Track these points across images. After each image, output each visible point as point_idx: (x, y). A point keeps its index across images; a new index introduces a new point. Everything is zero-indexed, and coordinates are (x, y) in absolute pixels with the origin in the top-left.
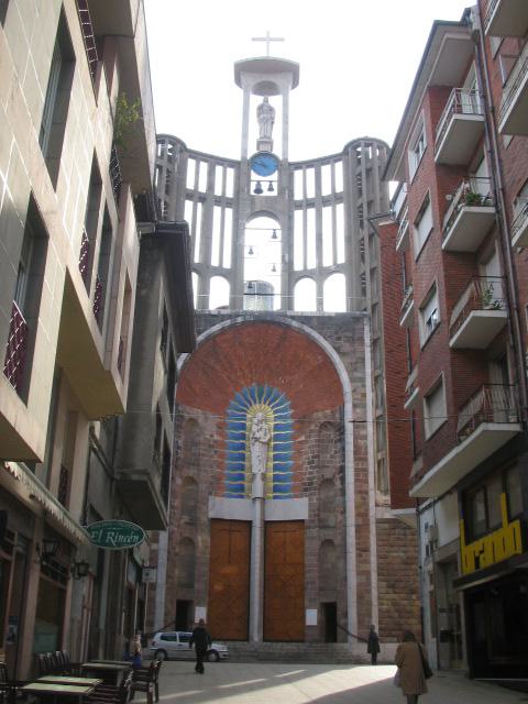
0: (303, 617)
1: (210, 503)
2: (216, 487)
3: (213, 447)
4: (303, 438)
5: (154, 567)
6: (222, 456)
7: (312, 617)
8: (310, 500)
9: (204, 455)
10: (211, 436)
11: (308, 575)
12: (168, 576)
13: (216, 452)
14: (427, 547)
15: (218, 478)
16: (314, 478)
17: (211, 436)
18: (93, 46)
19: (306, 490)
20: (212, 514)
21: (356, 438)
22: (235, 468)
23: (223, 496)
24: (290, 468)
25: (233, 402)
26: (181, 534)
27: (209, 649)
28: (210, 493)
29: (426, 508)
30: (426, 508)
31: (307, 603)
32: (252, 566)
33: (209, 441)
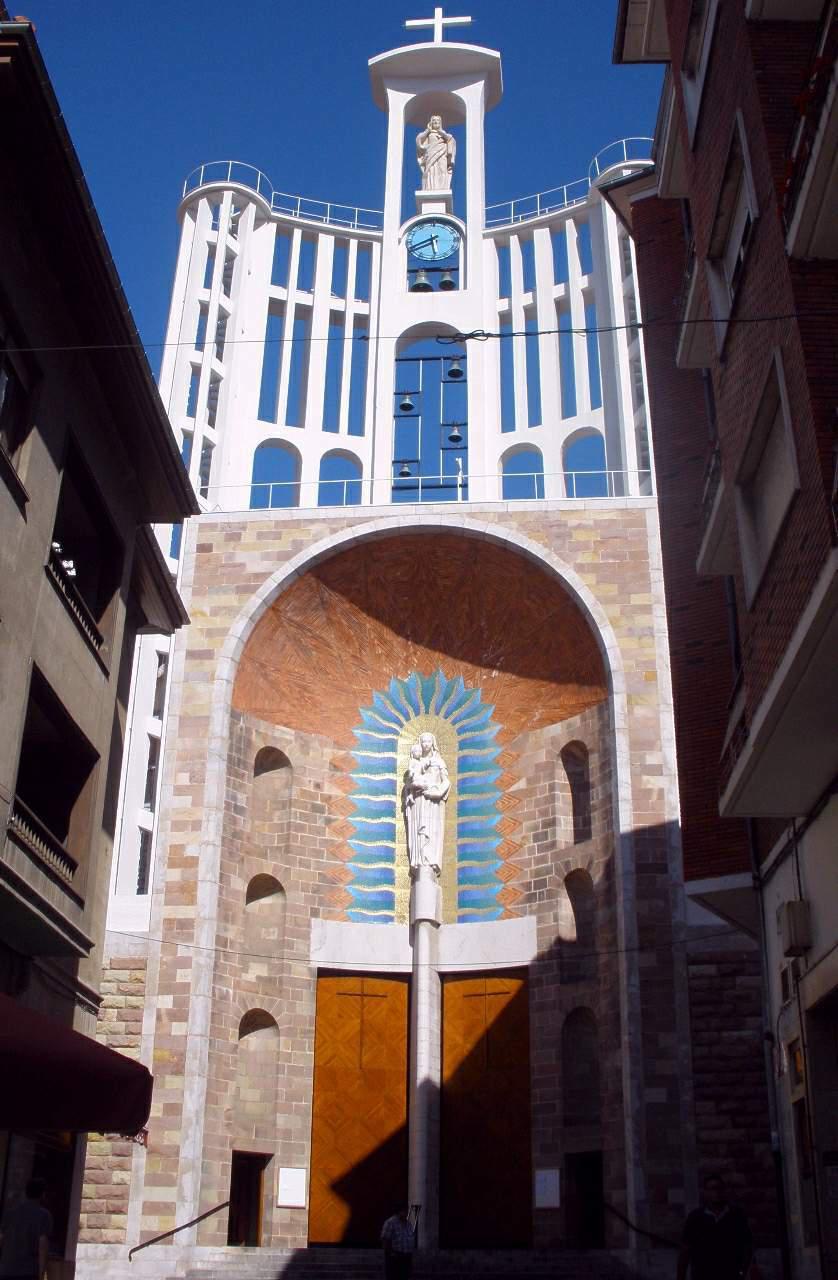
0: (527, 1188)
1: (315, 934)
2: (326, 898)
3: (320, 810)
4: (522, 784)
5: (179, 1070)
6: (336, 851)
7: (547, 1188)
8: (539, 921)
9: (301, 828)
10: (318, 786)
11: (536, 1091)
12: (211, 1098)
13: (328, 821)
14: (784, 975)
15: (330, 881)
16: (548, 871)
17: (318, 786)
18: (445, 39)
19: (530, 898)
20: (321, 959)
21: (635, 776)
22: (370, 858)
23: (347, 919)
24: (496, 855)
25: (367, 715)
26: (243, 1002)
27: (794, 161)
28: (315, 913)
29: (778, 863)
30: (778, 863)
31: (535, 1155)
32: (437, 1016)
33: (312, 796)
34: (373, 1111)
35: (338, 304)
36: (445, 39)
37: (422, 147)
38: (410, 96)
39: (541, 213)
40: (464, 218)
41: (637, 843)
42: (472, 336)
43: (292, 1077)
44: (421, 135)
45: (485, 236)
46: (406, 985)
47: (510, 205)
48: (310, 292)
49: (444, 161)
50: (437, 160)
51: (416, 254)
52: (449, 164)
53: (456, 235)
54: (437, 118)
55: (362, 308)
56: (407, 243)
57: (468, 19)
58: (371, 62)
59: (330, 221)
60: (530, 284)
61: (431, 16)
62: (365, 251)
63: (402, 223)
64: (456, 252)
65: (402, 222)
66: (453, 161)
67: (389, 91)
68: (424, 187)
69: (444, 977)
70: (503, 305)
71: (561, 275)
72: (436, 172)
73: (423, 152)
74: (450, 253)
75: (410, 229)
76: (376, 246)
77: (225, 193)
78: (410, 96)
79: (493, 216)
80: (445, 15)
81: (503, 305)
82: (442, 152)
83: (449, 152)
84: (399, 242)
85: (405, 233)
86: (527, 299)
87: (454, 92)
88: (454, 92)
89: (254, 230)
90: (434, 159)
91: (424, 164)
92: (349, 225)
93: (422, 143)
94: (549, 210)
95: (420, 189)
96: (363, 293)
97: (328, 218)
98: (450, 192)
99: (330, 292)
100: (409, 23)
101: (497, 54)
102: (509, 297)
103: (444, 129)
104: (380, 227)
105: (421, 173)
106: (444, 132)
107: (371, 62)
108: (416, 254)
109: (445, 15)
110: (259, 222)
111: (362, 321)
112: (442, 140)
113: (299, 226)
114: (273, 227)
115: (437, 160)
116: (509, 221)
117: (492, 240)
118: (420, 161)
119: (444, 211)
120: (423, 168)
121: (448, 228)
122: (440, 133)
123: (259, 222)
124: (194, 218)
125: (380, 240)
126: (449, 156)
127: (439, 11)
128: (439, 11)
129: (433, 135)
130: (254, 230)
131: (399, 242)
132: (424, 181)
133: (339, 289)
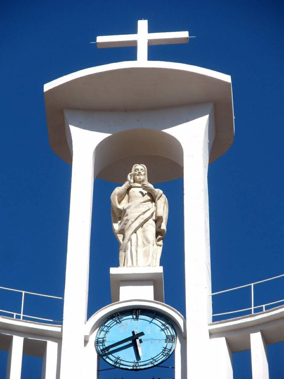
36: (152, 56)
37: (120, 207)
38: (102, 136)
39: (256, 311)
40: (182, 308)
43: (163, 194)
44: (118, 190)
45: (212, 334)
47: (251, 286)
49: (151, 228)
50: (142, 225)
51: (110, 360)
52: (158, 233)
53: (170, 332)
54: (140, 167)
56: (97, 343)
57: (185, 34)
58: (48, 87)
59: (24, 318)
61: (134, 30)
64: (171, 357)
65: (90, 313)
66: (164, 226)
67: (69, 125)
68: (121, 263)
73: (122, 214)
74: (161, 358)
75: (102, 323)
76: (51, 347)
77: (60, 329)
78: (102, 136)
82: (148, 214)
84: (86, 342)
85: (93, 330)
87: (164, 131)
88: (164, 131)
91: (122, 231)
92: (12, 316)
93: (120, 202)
94: (267, 308)
95: (117, 265)
97: (22, 315)
98: (160, 270)
100: (100, 39)
101: (227, 78)
103: (149, 181)
104: (58, 319)
105: (118, 244)
106: (151, 186)
107: (48, 87)
108: (110, 360)
112: (147, 197)
113: (19, 331)
115: (142, 225)
116: (250, 312)
117: (223, 339)
118: (116, 227)
119: (152, 298)
120: (120, 237)
121: (158, 322)
122: (145, 188)
125: (58, 338)
126: (158, 220)
127: (143, 25)
128: (143, 25)
129: (135, 191)
131: (86, 342)
132: (122, 254)
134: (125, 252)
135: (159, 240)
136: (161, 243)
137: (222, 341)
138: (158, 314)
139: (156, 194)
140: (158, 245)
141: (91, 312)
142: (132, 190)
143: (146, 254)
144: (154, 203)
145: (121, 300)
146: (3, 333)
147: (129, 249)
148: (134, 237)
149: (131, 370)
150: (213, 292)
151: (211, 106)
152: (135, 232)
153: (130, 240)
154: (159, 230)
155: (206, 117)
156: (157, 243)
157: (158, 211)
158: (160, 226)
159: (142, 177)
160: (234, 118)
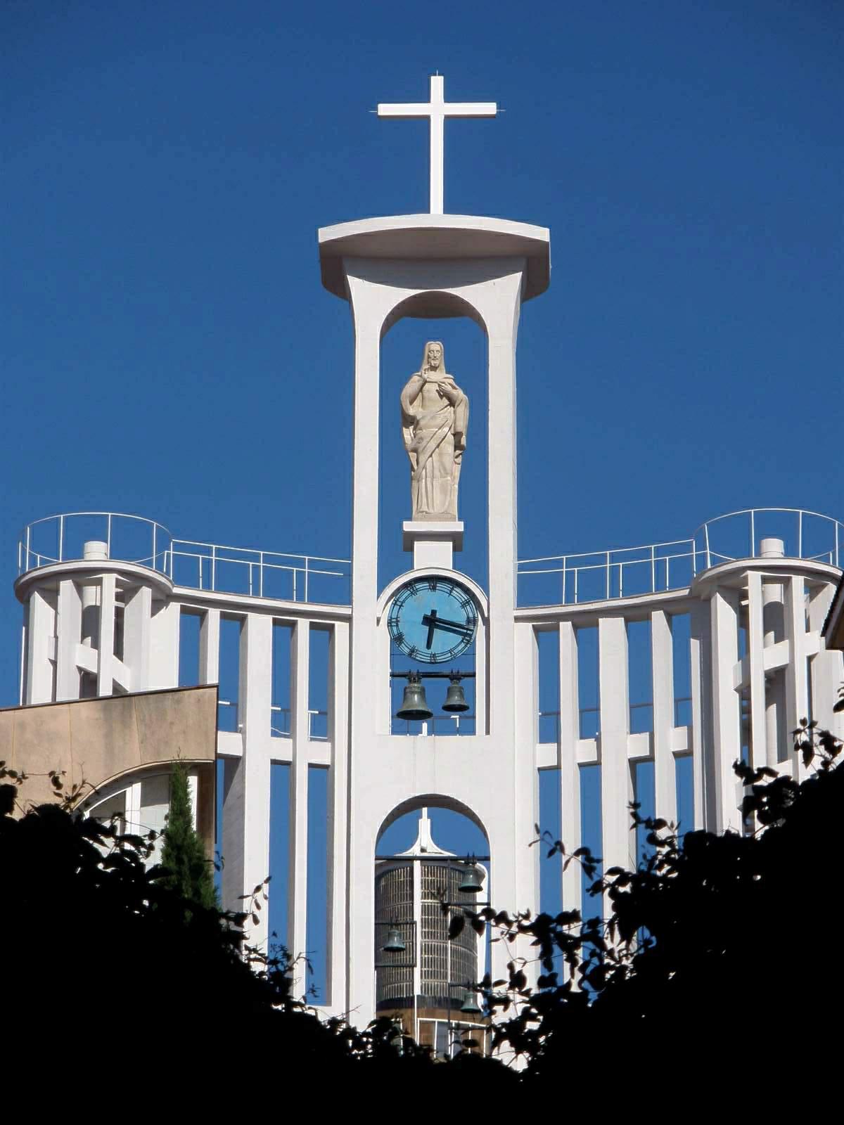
34: (80, 801)
35: (282, 749)
41: (783, 636)
42: (516, 1057)
45: (517, 619)
46: (218, 752)
48: (236, 730)
49: (448, 447)
52: (457, 446)
55: (320, 752)
60: (590, 725)
62: (323, 632)
63: (380, 590)
66: (464, 441)
67: (348, 276)
69: (311, 766)
70: (546, 755)
71: (641, 718)
72: (437, 473)
73: (411, 421)
76: (340, 628)
79: (528, 592)
80: (449, 97)
81: (546, 755)
83: (459, 429)
84: (378, 620)
86: (583, 751)
89: (153, 614)
90: (433, 444)
93: (411, 403)
95: (410, 519)
96: (322, 727)
99: (269, 728)
102: (557, 740)
104: (347, 600)
109: (449, 97)
110: (157, 605)
111: (320, 773)
112: (446, 402)
114: (175, 607)
120: (413, 456)
123: (157, 605)
124: (53, 603)
126: (457, 435)
129: (431, 389)
130: (153, 614)
131: (378, 620)
132: (415, 483)
133: (282, 723)
134: (418, 481)
135: (457, 457)
136: (459, 460)
137: (529, 626)
138: (445, 469)
139: (455, 399)
140: (456, 463)
141: (382, 586)
142: (427, 385)
143: (444, 490)
144: (452, 408)
145: (415, 568)
146: (397, 855)
147: (424, 481)
148: (429, 464)
149: (428, 663)
150: (520, 558)
151: (524, 263)
152: (431, 456)
153: (425, 467)
154: (457, 445)
155: (519, 275)
156: (456, 460)
157: (458, 423)
158: (460, 441)
159: (437, 362)
160: (551, 267)
